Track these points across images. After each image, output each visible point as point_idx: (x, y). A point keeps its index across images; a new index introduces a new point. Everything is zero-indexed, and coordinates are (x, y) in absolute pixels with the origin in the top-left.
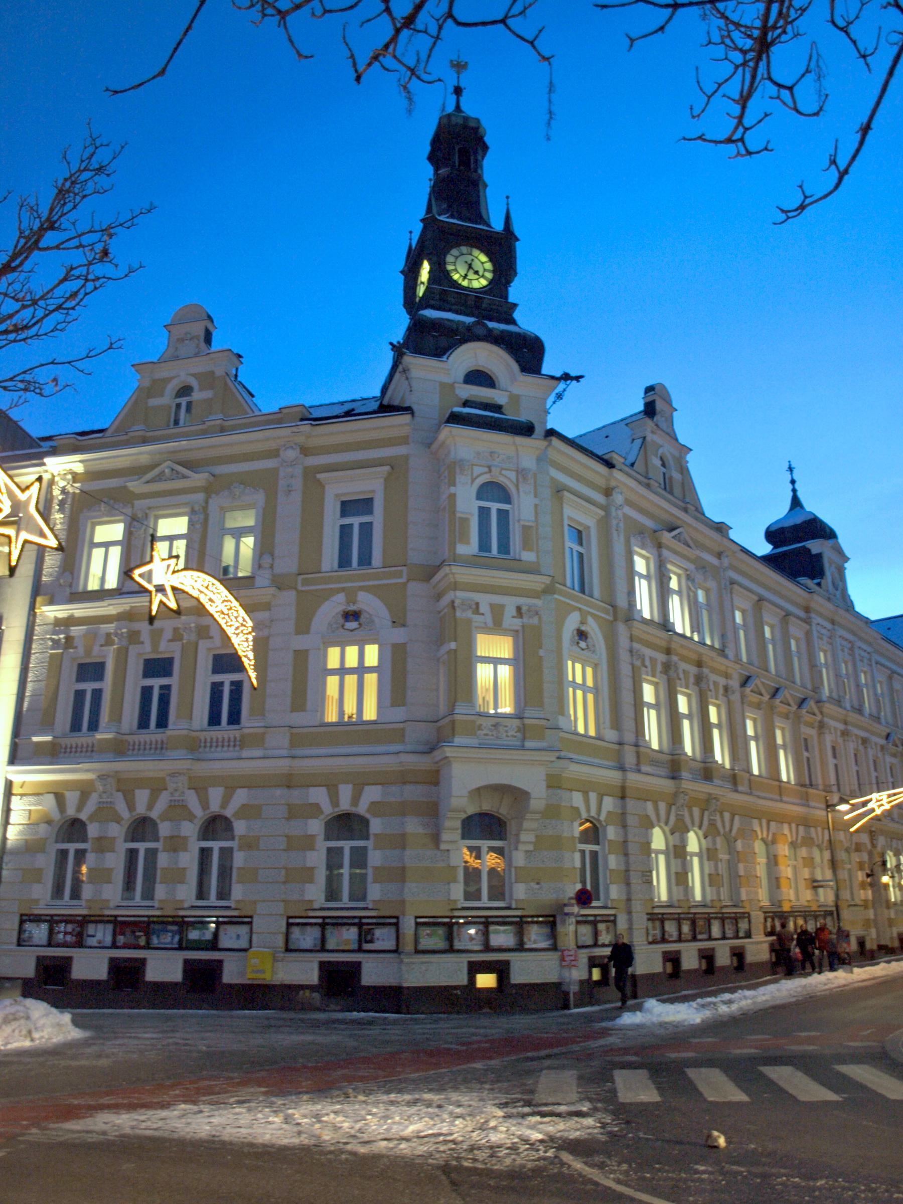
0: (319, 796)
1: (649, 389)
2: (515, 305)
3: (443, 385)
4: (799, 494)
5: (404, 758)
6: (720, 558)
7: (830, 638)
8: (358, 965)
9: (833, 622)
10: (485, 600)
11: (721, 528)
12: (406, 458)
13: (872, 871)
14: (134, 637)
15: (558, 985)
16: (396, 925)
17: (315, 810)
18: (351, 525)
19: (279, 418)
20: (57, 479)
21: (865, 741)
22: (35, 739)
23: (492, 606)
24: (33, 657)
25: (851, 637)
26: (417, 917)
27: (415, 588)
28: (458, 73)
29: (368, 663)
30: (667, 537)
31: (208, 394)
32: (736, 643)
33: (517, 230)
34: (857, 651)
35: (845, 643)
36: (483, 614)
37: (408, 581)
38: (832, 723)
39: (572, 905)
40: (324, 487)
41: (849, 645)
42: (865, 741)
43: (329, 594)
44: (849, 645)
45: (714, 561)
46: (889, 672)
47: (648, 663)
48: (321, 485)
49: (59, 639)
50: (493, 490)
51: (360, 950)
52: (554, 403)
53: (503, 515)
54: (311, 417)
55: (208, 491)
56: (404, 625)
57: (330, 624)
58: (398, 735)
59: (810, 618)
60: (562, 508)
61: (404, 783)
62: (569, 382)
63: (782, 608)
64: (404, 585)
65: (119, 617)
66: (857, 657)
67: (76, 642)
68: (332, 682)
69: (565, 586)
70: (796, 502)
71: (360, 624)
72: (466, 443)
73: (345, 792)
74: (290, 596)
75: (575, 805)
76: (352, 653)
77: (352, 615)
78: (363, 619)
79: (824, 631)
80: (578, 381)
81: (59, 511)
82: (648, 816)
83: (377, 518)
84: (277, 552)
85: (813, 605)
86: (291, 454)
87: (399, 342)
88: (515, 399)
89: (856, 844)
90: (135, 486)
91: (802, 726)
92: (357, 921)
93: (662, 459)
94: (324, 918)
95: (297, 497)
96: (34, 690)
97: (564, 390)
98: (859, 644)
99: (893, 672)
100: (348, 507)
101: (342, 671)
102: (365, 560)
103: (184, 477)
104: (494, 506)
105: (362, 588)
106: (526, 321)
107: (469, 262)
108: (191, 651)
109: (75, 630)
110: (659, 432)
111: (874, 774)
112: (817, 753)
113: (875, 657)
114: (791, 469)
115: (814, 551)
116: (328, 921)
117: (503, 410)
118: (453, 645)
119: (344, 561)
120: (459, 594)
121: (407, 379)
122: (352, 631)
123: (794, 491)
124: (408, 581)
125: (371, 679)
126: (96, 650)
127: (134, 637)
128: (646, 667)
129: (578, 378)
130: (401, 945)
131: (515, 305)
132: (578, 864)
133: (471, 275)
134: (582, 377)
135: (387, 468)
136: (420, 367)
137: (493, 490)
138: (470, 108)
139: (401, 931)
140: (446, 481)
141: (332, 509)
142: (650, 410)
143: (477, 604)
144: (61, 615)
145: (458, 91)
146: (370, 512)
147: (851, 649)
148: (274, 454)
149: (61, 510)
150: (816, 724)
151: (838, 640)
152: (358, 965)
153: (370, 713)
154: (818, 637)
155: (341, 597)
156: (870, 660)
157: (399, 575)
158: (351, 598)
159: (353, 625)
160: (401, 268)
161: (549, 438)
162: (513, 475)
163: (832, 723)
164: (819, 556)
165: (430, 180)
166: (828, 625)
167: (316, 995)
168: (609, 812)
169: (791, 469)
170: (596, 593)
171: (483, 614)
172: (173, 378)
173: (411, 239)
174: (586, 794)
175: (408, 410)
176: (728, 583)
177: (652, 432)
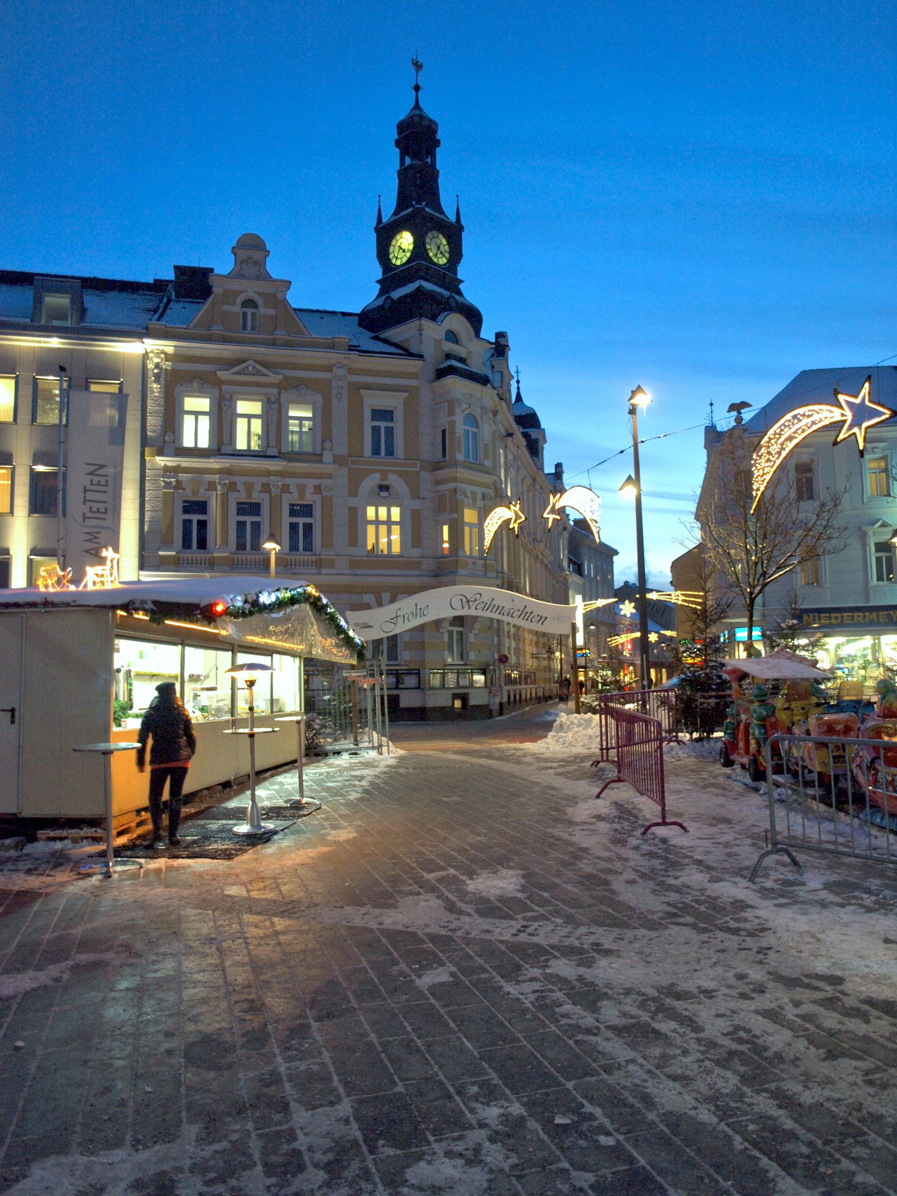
4: (521, 391)
10: (469, 488)
12: (417, 388)
14: (232, 487)
15: (488, 706)
16: (419, 674)
20: (151, 355)
22: (161, 553)
24: (147, 493)
27: (424, 475)
29: (393, 519)
31: (272, 312)
32: (268, 431)
33: (463, 222)
48: (361, 399)
49: (171, 482)
51: (397, 688)
55: (282, 387)
58: (417, 565)
64: (418, 473)
65: (221, 471)
67: (184, 485)
68: (371, 529)
74: (344, 471)
76: (383, 511)
77: (383, 488)
81: (155, 382)
84: (334, 441)
86: (341, 372)
90: (223, 375)
95: (345, 402)
96: (152, 518)
101: (377, 522)
102: (390, 452)
103: (263, 375)
105: (395, 472)
108: (275, 502)
109: (183, 476)
117: (467, 362)
119: (376, 451)
120: (458, 484)
124: (421, 471)
125: (396, 529)
126: (202, 491)
127: (232, 487)
130: (422, 682)
131: (378, 282)
133: (439, 255)
135: (406, 394)
141: (367, 415)
144: (169, 464)
148: (330, 369)
149: (157, 381)
153: (396, 549)
157: (415, 465)
158: (384, 477)
162: (479, 410)
172: (242, 292)
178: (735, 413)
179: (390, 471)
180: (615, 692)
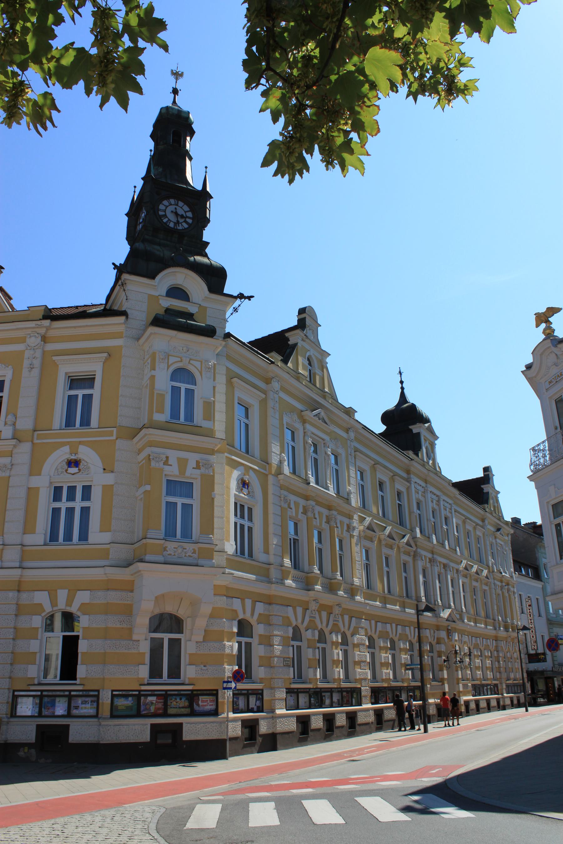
0: (42, 598)
1: (302, 311)
2: (208, 243)
3: (150, 296)
4: (405, 391)
5: (109, 570)
6: (348, 433)
7: (424, 492)
8: (67, 727)
9: (426, 482)
11: (350, 412)
13: (448, 657)
16: (98, 696)
17: (37, 609)
18: (77, 396)
19: (27, 316)
21: (445, 566)
23: (179, 460)
25: (438, 493)
26: (112, 691)
28: (177, 79)
30: (309, 415)
34: (442, 503)
35: (434, 497)
36: (171, 465)
37: (117, 439)
38: (423, 553)
39: (231, 682)
40: (57, 366)
41: (437, 499)
42: (445, 566)
43: (56, 446)
44: (437, 499)
45: (344, 435)
46: (475, 524)
47: (292, 506)
50: (181, 374)
52: (232, 314)
53: (190, 393)
54: (51, 315)
56: (112, 472)
57: (57, 469)
59: (410, 478)
60: (376, 475)
61: (108, 589)
62: (243, 300)
63: (391, 471)
66: (442, 506)
69: (234, 447)
70: (403, 395)
71: (79, 470)
72: (164, 339)
73: (62, 595)
75: (234, 608)
78: (81, 466)
79: (419, 488)
80: (250, 300)
82: (288, 618)
83: (96, 392)
85: (412, 469)
87: (120, 264)
88: (203, 309)
89: (437, 638)
91: (402, 554)
92: (67, 693)
93: (308, 360)
94: (42, 691)
95: (36, 372)
97: (239, 305)
98: (443, 497)
99: (467, 518)
100: (75, 382)
102: (86, 422)
104: (183, 387)
106: (215, 255)
107: (174, 211)
110: (307, 340)
111: (386, 569)
112: (489, 600)
113: (454, 507)
114: (400, 373)
115: (415, 431)
116: (45, 693)
118: (148, 488)
119: (69, 422)
121: (124, 290)
122: (73, 474)
123: (402, 388)
124: (117, 439)
128: (291, 509)
129: (249, 298)
131: (208, 243)
132: (291, 656)
134: (253, 297)
135: (105, 355)
136: (137, 285)
137: (181, 374)
138: (183, 103)
139: (100, 701)
140: (149, 366)
141: (61, 383)
142: (301, 324)
143: (167, 458)
145: (175, 91)
146: (92, 387)
147: (438, 501)
148: (22, 340)
150: (412, 553)
151: (429, 495)
152: (67, 727)
154: (444, 509)
155: (67, 449)
156: (451, 509)
158: (74, 450)
159: (74, 470)
160: (126, 212)
161: (226, 340)
163: (423, 553)
164: (418, 434)
165: (151, 151)
166: (423, 484)
167: (33, 751)
168: (260, 614)
169: (400, 373)
170: (475, 558)
171: (171, 465)
173: (135, 192)
174: (243, 600)
175: (123, 313)
176: (353, 451)
177: (303, 340)
178: (543, 325)
179: (80, 443)
180: (458, 659)
